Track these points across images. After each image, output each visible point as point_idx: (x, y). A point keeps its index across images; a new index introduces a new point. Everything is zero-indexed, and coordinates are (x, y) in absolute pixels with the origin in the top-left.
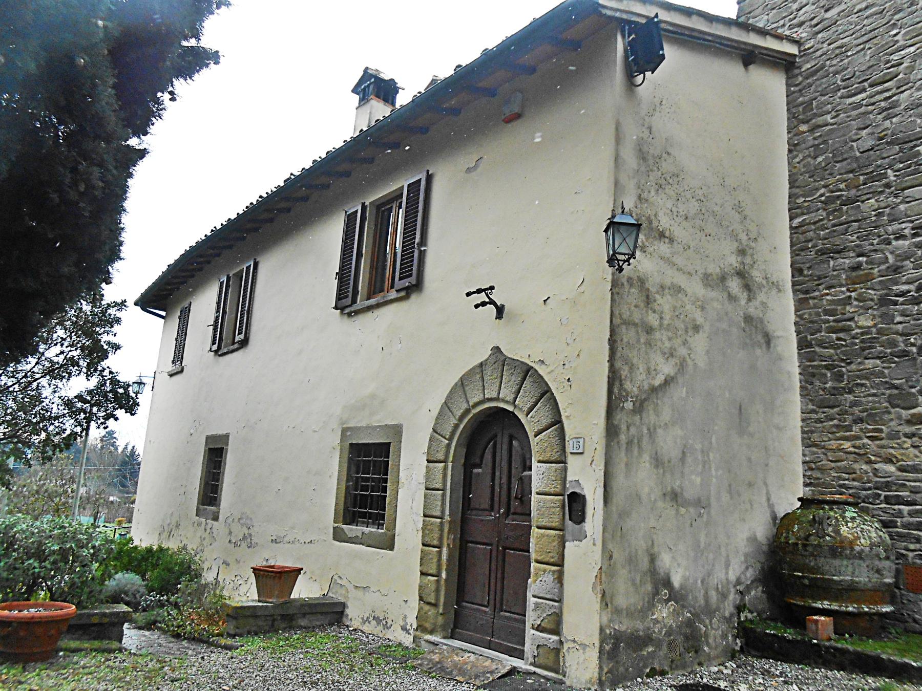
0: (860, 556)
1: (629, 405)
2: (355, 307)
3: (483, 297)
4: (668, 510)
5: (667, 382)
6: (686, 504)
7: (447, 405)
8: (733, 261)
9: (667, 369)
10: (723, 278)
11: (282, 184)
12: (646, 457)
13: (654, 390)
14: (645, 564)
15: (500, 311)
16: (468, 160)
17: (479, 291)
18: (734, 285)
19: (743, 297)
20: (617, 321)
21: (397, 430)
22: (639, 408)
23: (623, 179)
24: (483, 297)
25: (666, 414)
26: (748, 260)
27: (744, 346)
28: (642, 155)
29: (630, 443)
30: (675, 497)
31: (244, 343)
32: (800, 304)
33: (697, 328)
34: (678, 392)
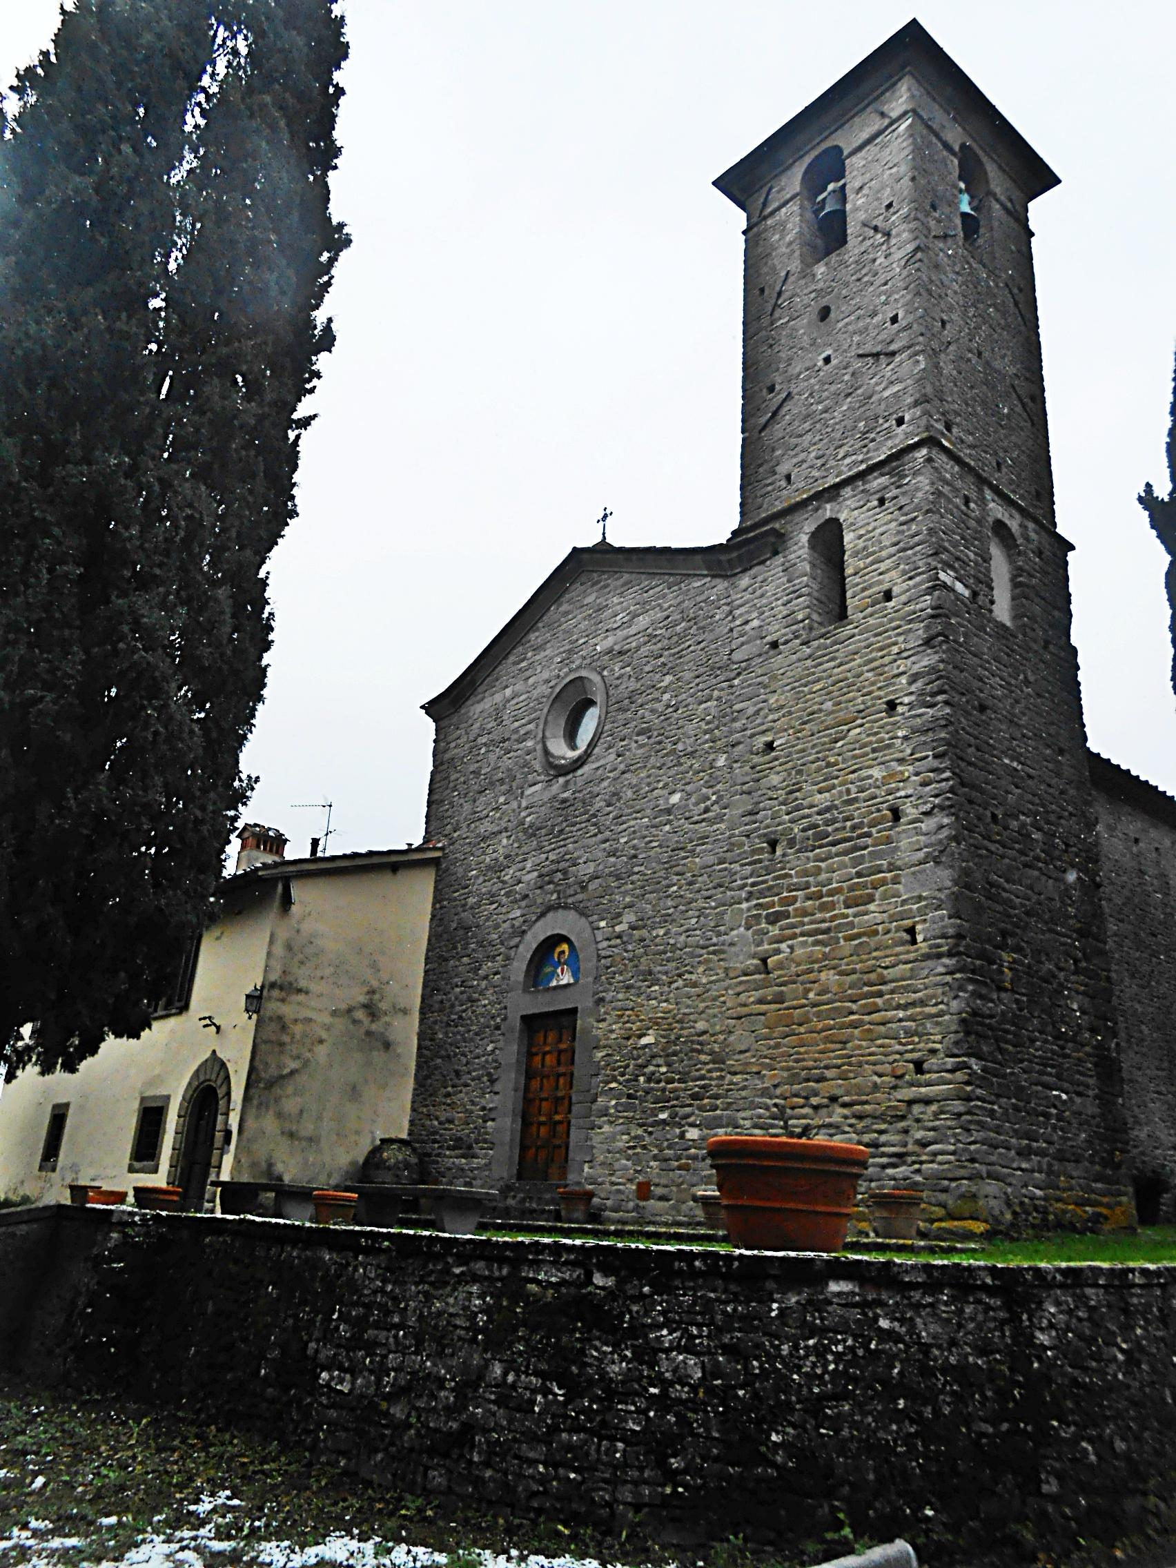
0: (389, 1168)
1: (262, 1085)
2: (156, 1015)
3: (207, 1021)
4: (284, 1143)
5: (292, 1073)
6: (300, 1139)
7: (190, 1083)
8: (362, 999)
9: (293, 1065)
10: (350, 1010)
11: (267, 658)
12: (271, 1112)
13: (282, 1077)
14: (264, 1165)
15: (218, 1028)
16: (218, 933)
17: (204, 1018)
18: (360, 1014)
19: (366, 1021)
20: (258, 1040)
21: (168, 1098)
22: (270, 1085)
23: (273, 963)
24: (207, 1021)
25: (290, 1090)
26: (377, 997)
27: (361, 1050)
28: (289, 947)
29: (261, 1104)
30: (291, 1135)
31: (587, 565)
32: (421, 1021)
33: (321, 1041)
34: (301, 1079)
